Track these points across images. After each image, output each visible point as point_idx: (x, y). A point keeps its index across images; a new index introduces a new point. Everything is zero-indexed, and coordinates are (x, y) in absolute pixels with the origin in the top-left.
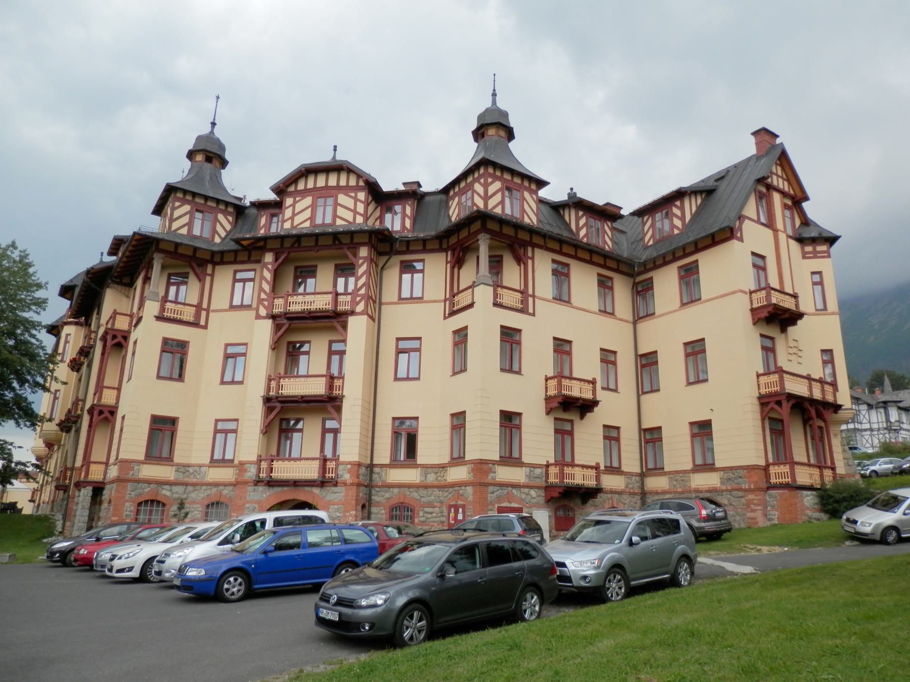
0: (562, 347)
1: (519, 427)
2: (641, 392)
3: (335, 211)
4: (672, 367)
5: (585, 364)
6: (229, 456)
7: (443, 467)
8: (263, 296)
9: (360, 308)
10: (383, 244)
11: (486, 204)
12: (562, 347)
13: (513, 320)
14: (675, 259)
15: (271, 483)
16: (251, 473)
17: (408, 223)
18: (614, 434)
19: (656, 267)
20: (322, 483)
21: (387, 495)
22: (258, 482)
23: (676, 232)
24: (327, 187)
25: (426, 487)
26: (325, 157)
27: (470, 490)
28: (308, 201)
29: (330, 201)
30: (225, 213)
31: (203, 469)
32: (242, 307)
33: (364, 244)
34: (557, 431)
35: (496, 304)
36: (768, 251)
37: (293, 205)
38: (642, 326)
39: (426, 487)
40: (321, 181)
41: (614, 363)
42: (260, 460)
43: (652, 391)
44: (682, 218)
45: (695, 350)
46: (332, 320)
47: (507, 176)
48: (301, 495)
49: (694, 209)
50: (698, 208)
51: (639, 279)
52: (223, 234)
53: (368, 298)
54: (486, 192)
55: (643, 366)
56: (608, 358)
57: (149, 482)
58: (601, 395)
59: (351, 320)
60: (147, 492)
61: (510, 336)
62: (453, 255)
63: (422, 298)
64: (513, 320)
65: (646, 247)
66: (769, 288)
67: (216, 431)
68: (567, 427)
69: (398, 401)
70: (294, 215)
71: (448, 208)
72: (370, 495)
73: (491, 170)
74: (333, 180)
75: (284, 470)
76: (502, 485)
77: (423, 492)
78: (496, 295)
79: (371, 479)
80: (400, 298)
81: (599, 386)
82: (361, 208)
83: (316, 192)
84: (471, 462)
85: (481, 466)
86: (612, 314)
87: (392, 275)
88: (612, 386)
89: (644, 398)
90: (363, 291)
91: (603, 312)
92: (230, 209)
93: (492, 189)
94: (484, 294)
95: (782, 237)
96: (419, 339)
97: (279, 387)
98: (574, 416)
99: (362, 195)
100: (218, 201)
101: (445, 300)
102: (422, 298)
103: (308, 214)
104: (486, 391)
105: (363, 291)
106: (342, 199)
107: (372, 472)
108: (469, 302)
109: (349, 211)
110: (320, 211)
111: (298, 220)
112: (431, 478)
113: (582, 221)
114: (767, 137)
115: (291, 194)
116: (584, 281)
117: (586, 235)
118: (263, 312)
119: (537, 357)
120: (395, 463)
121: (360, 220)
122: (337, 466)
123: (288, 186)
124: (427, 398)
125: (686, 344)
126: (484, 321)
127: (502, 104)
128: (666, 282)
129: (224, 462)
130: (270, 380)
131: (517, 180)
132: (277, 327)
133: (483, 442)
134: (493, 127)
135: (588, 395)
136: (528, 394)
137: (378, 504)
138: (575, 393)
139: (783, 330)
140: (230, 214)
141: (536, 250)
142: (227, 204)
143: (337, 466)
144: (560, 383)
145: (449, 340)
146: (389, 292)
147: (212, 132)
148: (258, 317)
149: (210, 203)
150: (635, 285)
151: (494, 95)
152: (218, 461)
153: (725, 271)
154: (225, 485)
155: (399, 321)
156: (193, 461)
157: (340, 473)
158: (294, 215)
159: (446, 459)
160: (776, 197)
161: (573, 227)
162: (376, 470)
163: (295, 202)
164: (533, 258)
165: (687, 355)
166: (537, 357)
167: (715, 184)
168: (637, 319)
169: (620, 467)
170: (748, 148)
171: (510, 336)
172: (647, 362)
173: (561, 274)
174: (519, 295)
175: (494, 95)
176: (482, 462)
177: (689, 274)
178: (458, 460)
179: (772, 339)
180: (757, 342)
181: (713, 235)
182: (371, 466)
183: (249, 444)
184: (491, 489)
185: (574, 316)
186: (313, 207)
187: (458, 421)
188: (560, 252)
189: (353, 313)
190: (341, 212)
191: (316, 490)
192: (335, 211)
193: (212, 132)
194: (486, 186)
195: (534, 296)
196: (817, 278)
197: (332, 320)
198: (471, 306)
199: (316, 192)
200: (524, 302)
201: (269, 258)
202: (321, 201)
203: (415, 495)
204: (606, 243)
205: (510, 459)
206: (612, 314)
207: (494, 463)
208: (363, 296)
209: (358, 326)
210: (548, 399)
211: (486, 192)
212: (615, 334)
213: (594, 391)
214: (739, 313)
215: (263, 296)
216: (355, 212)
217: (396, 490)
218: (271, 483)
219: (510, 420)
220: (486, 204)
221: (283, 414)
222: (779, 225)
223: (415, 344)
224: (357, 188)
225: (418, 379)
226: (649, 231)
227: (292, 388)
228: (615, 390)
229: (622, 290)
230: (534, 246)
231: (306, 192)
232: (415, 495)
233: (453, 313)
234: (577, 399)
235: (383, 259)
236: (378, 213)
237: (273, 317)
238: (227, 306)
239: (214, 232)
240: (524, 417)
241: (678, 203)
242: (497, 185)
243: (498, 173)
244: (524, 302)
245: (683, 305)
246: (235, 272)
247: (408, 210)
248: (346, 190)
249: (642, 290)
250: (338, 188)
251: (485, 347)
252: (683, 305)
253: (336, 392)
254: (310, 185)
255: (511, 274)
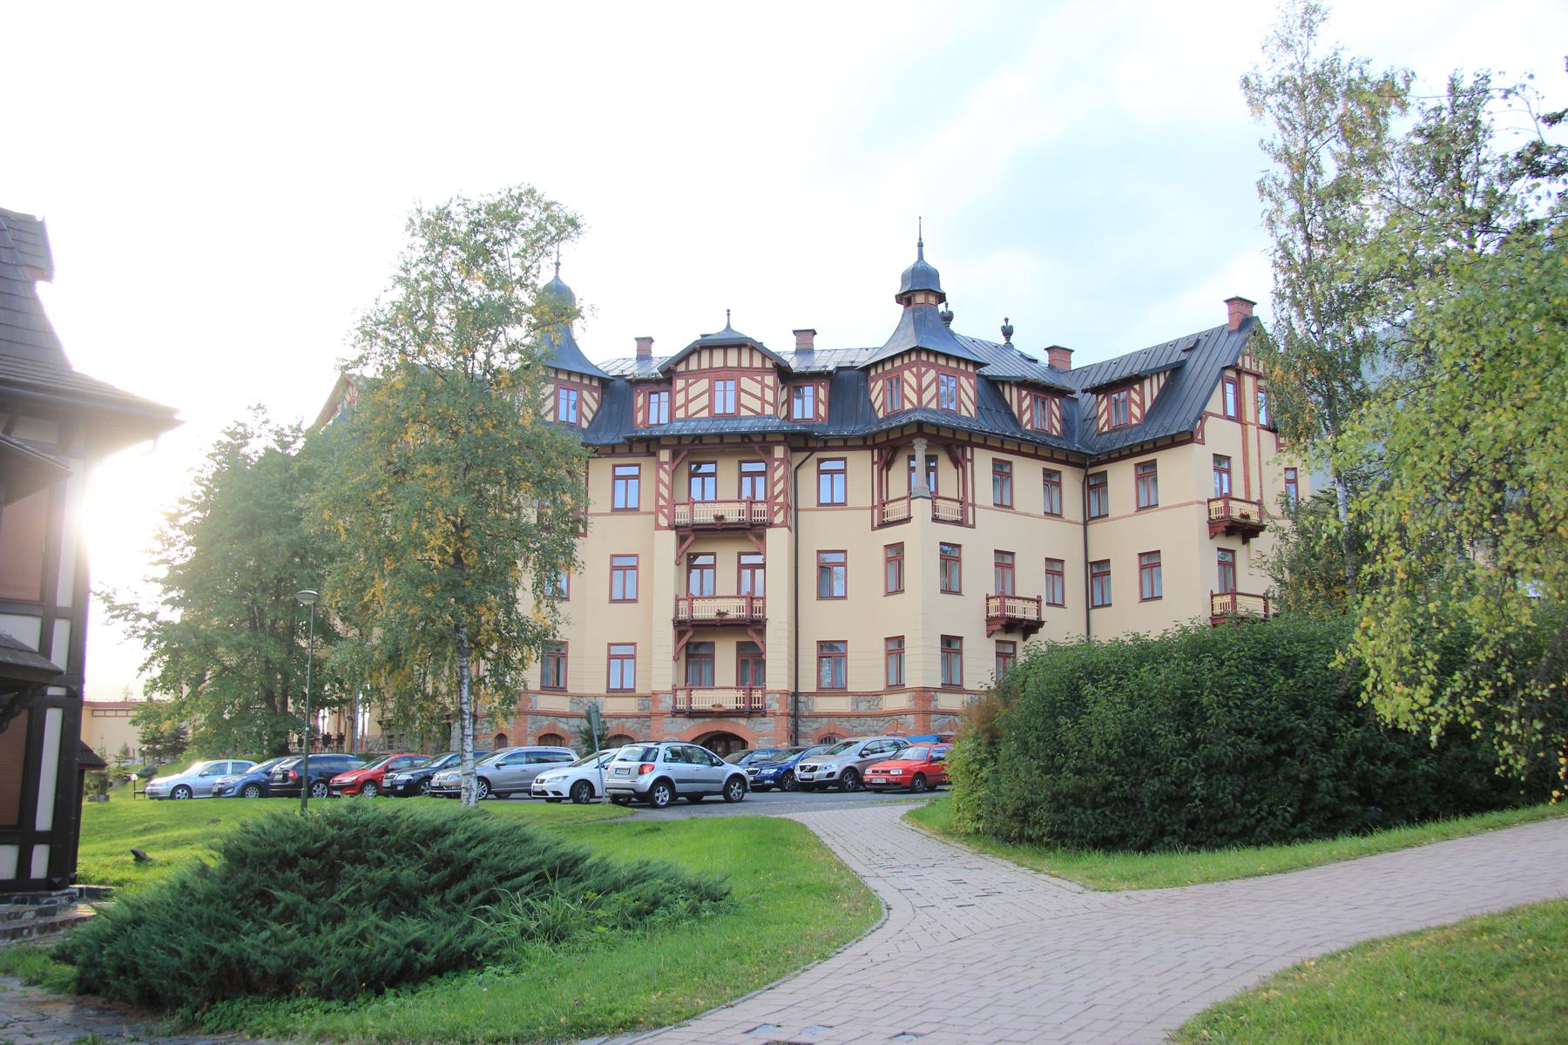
0: (1004, 560)
1: (959, 652)
2: (1090, 606)
3: (738, 399)
4: (1124, 578)
5: (1029, 580)
6: (628, 685)
7: (877, 694)
8: (662, 503)
9: (779, 519)
10: (802, 441)
11: (920, 400)
12: (1004, 560)
13: (953, 534)
14: (1132, 455)
15: (693, 714)
16: (666, 704)
17: (822, 410)
18: (1057, 568)
19: (1111, 460)
20: (751, 713)
21: (815, 726)
22: (676, 713)
23: (1134, 422)
24: (725, 368)
25: (858, 716)
26: (715, 327)
27: (911, 718)
28: (704, 384)
29: (731, 385)
30: (590, 389)
31: (600, 700)
32: (626, 510)
33: (778, 443)
34: (998, 654)
35: (935, 519)
36: (1233, 450)
37: (686, 389)
38: (1093, 528)
39: (858, 716)
40: (718, 359)
41: (1061, 574)
42: (675, 690)
43: (1103, 606)
44: (1141, 406)
45: (1150, 561)
46: (750, 531)
47: (942, 361)
48: (727, 726)
49: (1155, 393)
50: (1167, 380)
51: (1091, 471)
52: (590, 416)
53: (786, 507)
54: (920, 385)
55: (1093, 575)
56: (1054, 568)
57: (547, 714)
58: (1048, 614)
59: (770, 533)
60: (545, 725)
61: (950, 556)
62: (880, 456)
63: (844, 504)
64: (953, 534)
65: (1101, 434)
66: (1227, 498)
67: (611, 657)
68: (1009, 650)
69: (824, 622)
70: (688, 401)
71: (868, 392)
72: (796, 726)
73: (924, 357)
74: (732, 360)
75: (703, 699)
76: (944, 713)
77: (855, 722)
78: (935, 509)
79: (796, 708)
80: (820, 504)
81: (1043, 603)
82: (769, 395)
83: (714, 374)
84: (912, 690)
85: (925, 693)
86: (1060, 516)
87: (808, 474)
88: (1058, 601)
89: (1093, 613)
90: (781, 499)
91: (1050, 514)
92: (595, 383)
93: (926, 381)
94: (921, 509)
95: (1252, 430)
96: (845, 552)
97: (691, 608)
98: (1016, 637)
99: (770, 380)
100: (582, 375)
101: (873, 508)
102: (844, 504)
103: (704, 400)
104: (921, 614)
105: (781, 499)
106: (746, 383)
107: (797, 702)
108: (905, 515)
109: (755, 401)
110: (719, 396)
111: (693, 408)
112: (863, 707)
113: (1026, 403)
114: (1243, 308)
115: (681, 375)
116: (1028, 474)
117: (1031, 420)
118: (664, 522)
119: (978, 575)
120: (821, 692)
121: (769, 410)
122: (764, 695)
123: (677, 364)
124: (861, 618)
125: (1141, 555)
126: (921, 539)
127: (931, 260)
128: (1121, 477)
129: (623, 692)
130: (677, 600)
131: (953, 364)
132: (682, 540)
133: (922, 668)
134: (921, 292)
135: (1032, 616)
136: (967, 618)
137: (806, 736)
138: (1019, 615)
139: (1245, 541)
140: (595, 389)
141: (976, 450)
142: (591, 377)
143: (764, 695)
144: (1003, 603)
145: (880, 555)
146: (807, 498)
147: (557, 278)
148: (658, 527)
149: (573, 379)
150: (1087, 477)
151: (920, 245)
152: (615, 690)
153: (1185, 475)
154: (628, 717)
155: (822, 531)
156: (587, 691)
157: (768, 702)
158: (688, 401)
159: (881, 687)
160: (1248, 381)
161: (1015, 410)
162: (802, 699)
163: (688, 386)
164: (972, 461)
165: (1142, 567)
166: (978, 575)
167: (1184, 356)
168: (1088, 520)
169: (961, 685)
170: (1220, 317)
171: (950, 556)
172: (1098, 571)
173: (1002, 473)
174: (957, 506)
175: (920, 245)
176: (925, 690)
177: (1147, 473)
178: (896, 687)
179: (1233, 552)
180: (1214, 557)
181: (1173, 437)
182: (796, 694)
183: (660, 668)
184: (933, 717)
185: (1020, 520)
186: (711, 391)
187: (896, 646)
188: (1002, 450)
189: (771, 525)
190: (745, 399)
191: (743, 721)
192: (738, 399)
193: (557, 278)
194: (919, 377)
195: (973, 505)
196: (1290, 475)
197: (750, 531)
198: (908, 520)
199: (714, 374)
200: (963, 512)
201: (665, 455)
202: (719, 385)
203: (846, 725)
204: (1052, 425)
205: (951, 687)
206: (1060, 516)
207: (936, 690)
208: (782, 506)
209: (777, 541)
210: (990, 621)
211: (920, 385)
212: (1063, 540)
213: (1039, 611)
214: (1195, 522)
215: (662, 503)
216: (764, 401)
217: (825, 720)
218: (693, 714)
219: (950, 645)
220: (920, 400)
221: (695, 640)
222: (1249, 416)
223: (840, 558)
224: (764, 371)
225: (845, 598)
226: (1104, 413)
227: (705, 610)
228: (1062, 606)
229: (1071, 481)
230: (973, 445)
231: (700, 374)
232: (846, 725)
233: (884, 525)
234: (1021, 620)
235: (801, 456)
236: (783, 396)
237: (677, 528)
238: (609, 510)
239: (581, 414)
240: (965, 641)
241: (1137, 387)
242: (932, 374)
243: (932, 359)
244: (963, 512)
245: (1140, 509)
246: (614, 466)
247: (822, 393)
248: (750, 372)
249: (1095, 486)
250: (740, 370)
251: (922, 565)
252: (1140, 509)
253: (756, 615)
254: (705, 365)
255: (947, 475)
